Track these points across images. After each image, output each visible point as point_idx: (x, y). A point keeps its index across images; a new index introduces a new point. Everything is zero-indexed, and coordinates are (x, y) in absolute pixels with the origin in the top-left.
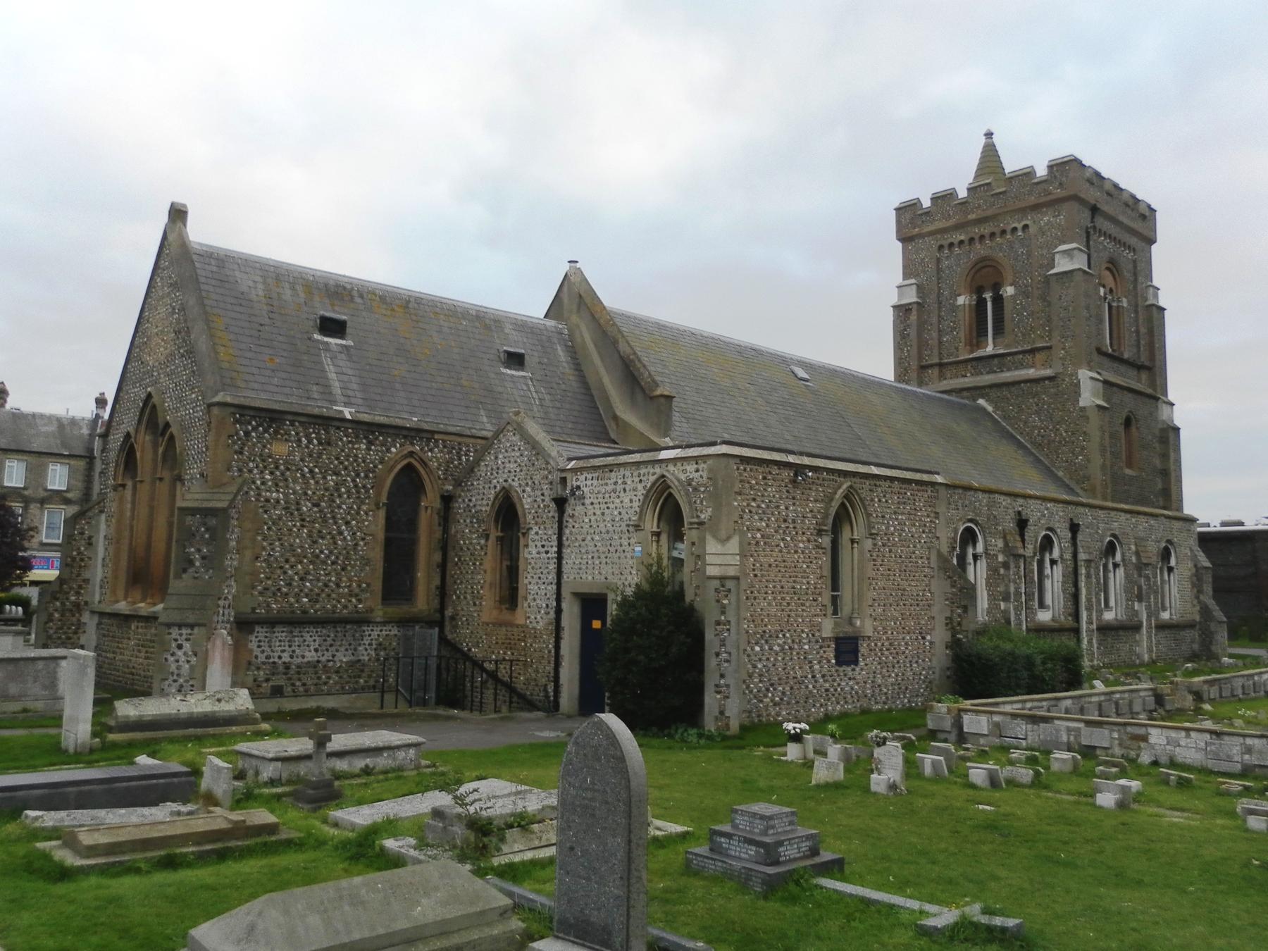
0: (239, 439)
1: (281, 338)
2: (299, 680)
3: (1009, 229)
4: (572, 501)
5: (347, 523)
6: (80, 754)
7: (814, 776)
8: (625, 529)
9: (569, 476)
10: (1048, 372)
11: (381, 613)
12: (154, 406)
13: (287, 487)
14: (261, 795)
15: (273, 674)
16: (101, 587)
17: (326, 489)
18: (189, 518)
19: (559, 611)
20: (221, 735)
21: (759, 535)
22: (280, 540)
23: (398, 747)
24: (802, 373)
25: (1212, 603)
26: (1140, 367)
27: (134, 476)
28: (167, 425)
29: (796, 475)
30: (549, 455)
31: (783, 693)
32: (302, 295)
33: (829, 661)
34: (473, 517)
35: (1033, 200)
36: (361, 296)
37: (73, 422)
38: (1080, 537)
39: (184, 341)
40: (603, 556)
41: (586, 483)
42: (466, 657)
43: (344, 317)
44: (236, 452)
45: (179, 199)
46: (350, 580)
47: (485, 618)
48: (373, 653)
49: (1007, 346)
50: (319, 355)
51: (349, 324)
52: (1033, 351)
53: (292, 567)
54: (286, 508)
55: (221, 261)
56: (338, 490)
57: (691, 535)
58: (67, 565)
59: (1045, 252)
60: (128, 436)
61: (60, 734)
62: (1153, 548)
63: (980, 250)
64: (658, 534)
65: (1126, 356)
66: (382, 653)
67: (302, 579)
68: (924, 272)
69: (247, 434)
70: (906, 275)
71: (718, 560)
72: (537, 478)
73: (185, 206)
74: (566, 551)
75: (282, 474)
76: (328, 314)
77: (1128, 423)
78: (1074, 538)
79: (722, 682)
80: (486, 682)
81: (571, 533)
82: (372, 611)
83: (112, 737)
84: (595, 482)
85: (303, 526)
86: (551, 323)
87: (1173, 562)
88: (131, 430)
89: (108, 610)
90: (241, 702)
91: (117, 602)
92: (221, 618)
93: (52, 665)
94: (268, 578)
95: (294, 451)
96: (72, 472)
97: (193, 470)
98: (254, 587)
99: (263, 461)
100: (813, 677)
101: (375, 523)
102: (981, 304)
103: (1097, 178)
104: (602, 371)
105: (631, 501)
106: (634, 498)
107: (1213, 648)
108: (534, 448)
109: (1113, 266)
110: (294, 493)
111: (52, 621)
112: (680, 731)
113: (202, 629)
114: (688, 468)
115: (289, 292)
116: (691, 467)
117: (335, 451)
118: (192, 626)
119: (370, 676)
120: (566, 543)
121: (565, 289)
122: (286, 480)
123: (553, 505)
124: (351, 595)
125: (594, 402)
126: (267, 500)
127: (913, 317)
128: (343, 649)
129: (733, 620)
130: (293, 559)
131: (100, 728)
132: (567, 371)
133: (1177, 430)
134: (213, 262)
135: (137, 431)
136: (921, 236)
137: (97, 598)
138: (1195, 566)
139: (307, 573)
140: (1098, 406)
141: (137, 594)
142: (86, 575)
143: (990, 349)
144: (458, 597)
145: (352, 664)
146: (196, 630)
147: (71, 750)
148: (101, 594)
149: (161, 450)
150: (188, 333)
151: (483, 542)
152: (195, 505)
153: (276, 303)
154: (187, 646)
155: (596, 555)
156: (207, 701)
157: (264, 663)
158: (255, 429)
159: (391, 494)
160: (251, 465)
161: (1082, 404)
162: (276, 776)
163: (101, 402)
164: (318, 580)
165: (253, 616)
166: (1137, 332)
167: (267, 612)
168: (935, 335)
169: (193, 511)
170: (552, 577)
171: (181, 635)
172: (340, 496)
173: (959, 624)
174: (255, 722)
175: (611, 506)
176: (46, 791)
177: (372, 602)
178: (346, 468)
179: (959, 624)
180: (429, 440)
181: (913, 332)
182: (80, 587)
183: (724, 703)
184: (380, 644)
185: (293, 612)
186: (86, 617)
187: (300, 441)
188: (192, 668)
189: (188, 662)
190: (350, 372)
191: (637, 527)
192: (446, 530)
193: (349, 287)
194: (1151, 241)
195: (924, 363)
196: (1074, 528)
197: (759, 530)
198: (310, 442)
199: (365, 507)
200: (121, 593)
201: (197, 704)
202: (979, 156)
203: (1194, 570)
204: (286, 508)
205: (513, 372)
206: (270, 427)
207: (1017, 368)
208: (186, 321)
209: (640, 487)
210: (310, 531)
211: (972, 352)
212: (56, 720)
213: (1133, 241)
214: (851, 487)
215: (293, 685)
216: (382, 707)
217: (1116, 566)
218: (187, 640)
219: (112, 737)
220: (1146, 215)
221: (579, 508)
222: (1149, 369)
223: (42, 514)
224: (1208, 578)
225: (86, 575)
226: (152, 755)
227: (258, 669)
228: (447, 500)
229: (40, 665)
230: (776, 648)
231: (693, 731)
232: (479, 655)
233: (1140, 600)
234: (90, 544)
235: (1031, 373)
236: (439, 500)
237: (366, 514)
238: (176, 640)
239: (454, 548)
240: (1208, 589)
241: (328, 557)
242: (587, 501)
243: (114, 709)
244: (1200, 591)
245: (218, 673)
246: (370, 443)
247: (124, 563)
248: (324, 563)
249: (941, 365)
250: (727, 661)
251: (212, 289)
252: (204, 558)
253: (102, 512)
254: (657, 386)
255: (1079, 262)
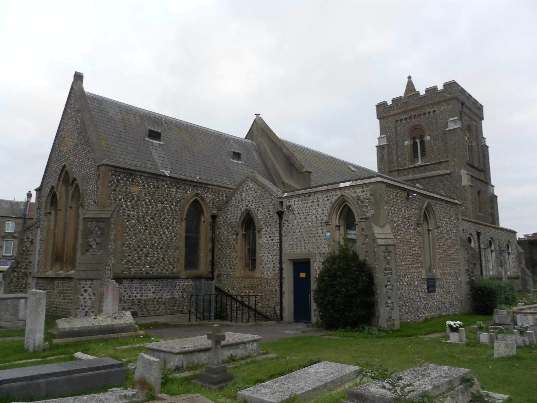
0: (114, 183)
1: (131, 139)
2: (145, 308)
3: (427, 112)
4: (287, 213)
5: (168, 228)
6: (37, 352)
7: (495, 352)
8: (319, 225)
9: (284, 201)
10: (447, 172)
11: (184, 273)
12: (67, 172)
13: (138, 209)
14: (176, 379)
15: (132, 305)
16: (38, 265)
17: (157, 211)
18: (90, 223)
19: (281, 269)
20: (118, 338)
21: (395, 225)
22: (135, 236)
23: (248, 342)
24: (353, 169)
25: (525, 267)
26: (480, 171)
27: (56, 210)
28: (75, 179)
29: (408, 195)
30: (272, 191)
31: (409, 307)
32: (139, 120)
33: (425, 291)
34: (229, 225)
35: (437, 99)
36: (166, 123)
37: (17, 203)
38: (481, 238)
39: (83, 137)
40: (306, 240)
41: (295, 203)
42: (227, 295)
43: (160, 131)
44: (113, 190)
45: (79, 71)
46: (169, 257)
47: (237, 275)
48: (181, 294)
49: (427, 162)
50: (149, 148)
51: (162, 135)
52: (439, 163)
53: (141, 250)
54: (138, 220)
55: (101, 103)
56: (163, 211)
57: (360, 225)
58: (20, 254)
59: (443, 121)
60: (53, 188)
61: (23, 341)
62: (504, 244)
63: (414, 122)
64: (339, 226)
65: (475, 166)
66: (185, 294)
67: (146, 256)
68: (390, 132)
69: (118, 181)
70: (381, 133)
71: (382, 236)
72: (265, 203)
73: (82, 74)
74: (284, 239)
75: (136, 202)
76: (152, 129)
77: (479, 193)
78: (478, 239)
79: (389, 301)
80: (239, 307)
81: (287, 229)
82: (180, 272)
83: (56, 341)
84: (300, 202)
85: (146, 229)
86: (249, 141)
87: (510, 251)
88: (54, 185)
89: (42, 276)
90: (127, 319)
91: (47, 272)
92: (106, 276)
93: (16, 302)
94: (129, 256)
95: (141, 191)
96: (17, 225)
97: (89, 201)
98: (122, 260)
99: (126, 195)
100: (420, 298)
101: (181, 228)
102: (415, 145)
103: (463, 91)
104: (275, 162)
105: (323, 210)
106: (324, 209)
107: (528, 287)
108: (263, 188)
109: (469, 128)
110: (142, 212)
111: (12, 282)
112: (367, 328)
113: (98, 281)
114: (357, 191)
115: (133, 118)
116: (359, 190)
117: (161, 192)
118: (92, 280)
119: (179, 306)
120: (284, 234)
121: (255, 126)
122: (138, 205)
123: (276, 216)
124: (170, 265)
125: (272, 176)
126: (129, 216)
127: (386, 150)
128: (166, 292)
129: (393, 267)
130: (141, 246)
131: (48, 337)
132: (259, 162)
133: (496, 197)
134: (96, 101)
135: (57, 185)
136: (388, 117)
137: (36, 270)
138: (518, 252)
139: (149, 253)
140: (470, 185)
141: (57, 266)
142: (30, 259)
143: (420, 163)
144: (222, 265)
145: (171, 300)
146: (95, 282)
147: (31, 350)
148: (38, 268)
149: (71, 193)
150: (86, 132)
151: (235, 237)
152: (93, 216)
153: (127, 123)
154: (90, 290)
155: (302, 239)
156: (109, 319)
157: (128, 300)
158: (122, 179)
159: (188, 215)
160: (120, 197)
161: (463, 184)
162: (180, 365)
163: (29, 195)
164: (154, 257)
165: (122, 275)
166: (479, 156)
167: (129, 272)
168: (395, 158)
169: (91, 220)
170: (277, 252)
171: (86, 284)
172: (164, 214)
173: (472, 272)
174: (135, 330)
175: (310, 213)
176: (24, 383)
177: (180, 268)
178: (166, 201)
179: (472, 272)
180: (205, 188)
181: (386, 157)
182: (27, 265)
183: (388, 312)
184: (184, 289)
185: (142, 273)
186: (30, 280)
187: (144, 186)
188: (92, 302)
189: (90, 299)
190: (164, 156)
191: (327, 223)
192: (213, 233)
193: (160, 118)
194: (482, 119)
195: (391, 170)
196: (478, 234)
197: (395, 222)
198: (149, 186)
199: (176, 220)
200: (49, 267)
201: (103, 321)
202: (406, 86)
203: (517, 254)
204: (138, 220)
205: (236, 161)
206: (130, 178)
207: (432, 171)
208: (84, 127)
209: (328, 202)
210: (150, 232)
211: (412, 165)
212: (21, 332)
213: (476, 118)
214: (429, 203)
215: (142, 311)
216: (189, 321)
217: (492, 251)
218: (90, 287)
219: (56, 341)
220: (480, 108)
221: (291, 216)
222: (484, 171)
223: (3, 243)
224: (523, 257)
225: (30, 259)
226: (85, 351)
227: (125, 302)
228: (214, 217)
229: (9, 302)
230: (405, 283)
231: (374, 328)
232: (234, 294)
233: (502, 266)
234: (32, 243)
235: (439, 172)
236: (210, 218)
237: (176, 223)
238: (84, 287)
239: (218, 241)
240: (523, 262)
241: (158, 245)
242: (296, 212)
243: (56, 324)
244: (520, 263)
245: (110, 304)
246: (178, 188)
247: (50, 252)
248: (157, 248)
249: (398, 170)
250: (392, 290)
251: (96, 114)
252: (97, 244)
253: (38, 227)
254: (304, 167)
255: (458, 125)
